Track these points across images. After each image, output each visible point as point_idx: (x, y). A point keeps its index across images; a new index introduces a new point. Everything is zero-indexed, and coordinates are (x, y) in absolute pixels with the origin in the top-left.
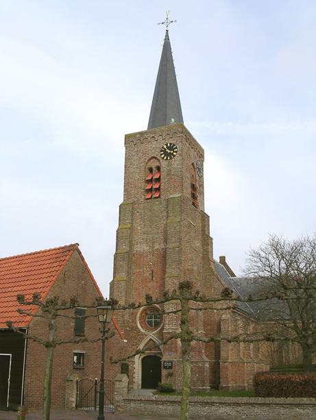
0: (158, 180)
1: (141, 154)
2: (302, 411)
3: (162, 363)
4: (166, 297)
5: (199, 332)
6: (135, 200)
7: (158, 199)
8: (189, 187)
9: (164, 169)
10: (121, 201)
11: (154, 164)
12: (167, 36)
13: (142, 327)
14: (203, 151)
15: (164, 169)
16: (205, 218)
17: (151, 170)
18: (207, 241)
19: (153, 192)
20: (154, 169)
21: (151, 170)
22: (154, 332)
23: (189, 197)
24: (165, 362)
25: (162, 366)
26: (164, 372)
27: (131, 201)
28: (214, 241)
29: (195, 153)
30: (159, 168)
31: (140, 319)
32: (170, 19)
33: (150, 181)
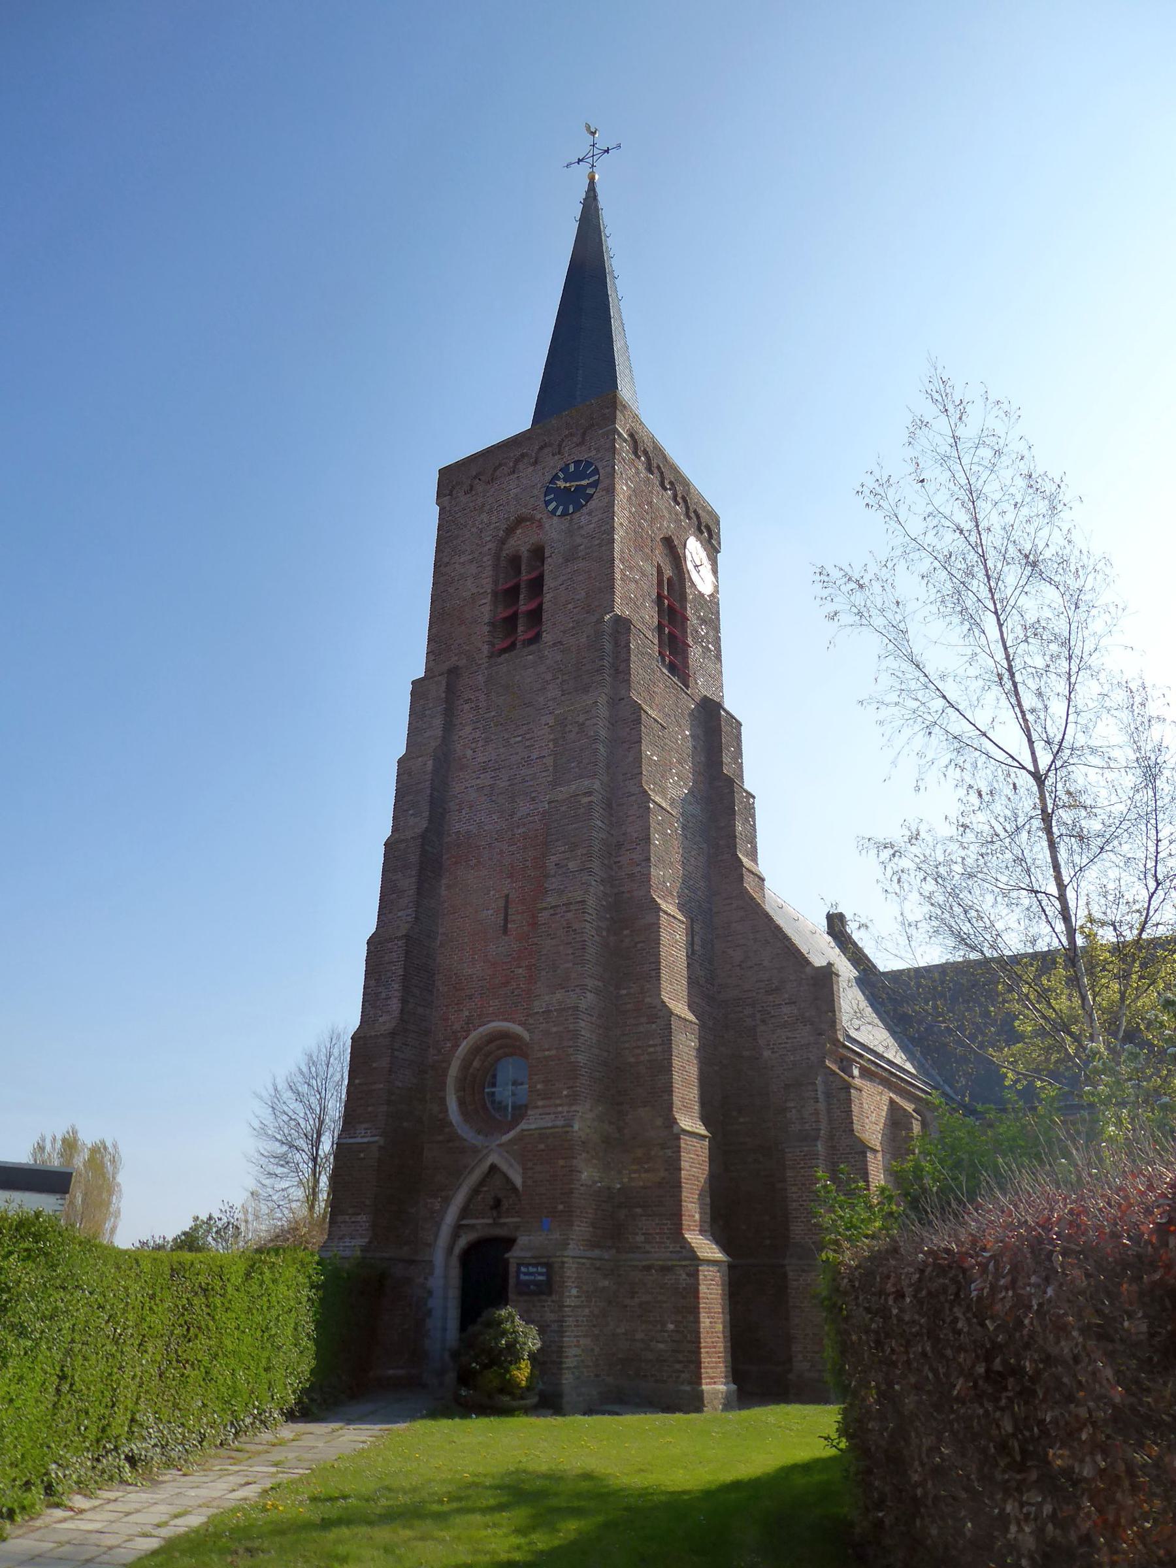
3: (512, 1269)
11: (521, 542)
22: (505, 1138)
25: (512, 1281)
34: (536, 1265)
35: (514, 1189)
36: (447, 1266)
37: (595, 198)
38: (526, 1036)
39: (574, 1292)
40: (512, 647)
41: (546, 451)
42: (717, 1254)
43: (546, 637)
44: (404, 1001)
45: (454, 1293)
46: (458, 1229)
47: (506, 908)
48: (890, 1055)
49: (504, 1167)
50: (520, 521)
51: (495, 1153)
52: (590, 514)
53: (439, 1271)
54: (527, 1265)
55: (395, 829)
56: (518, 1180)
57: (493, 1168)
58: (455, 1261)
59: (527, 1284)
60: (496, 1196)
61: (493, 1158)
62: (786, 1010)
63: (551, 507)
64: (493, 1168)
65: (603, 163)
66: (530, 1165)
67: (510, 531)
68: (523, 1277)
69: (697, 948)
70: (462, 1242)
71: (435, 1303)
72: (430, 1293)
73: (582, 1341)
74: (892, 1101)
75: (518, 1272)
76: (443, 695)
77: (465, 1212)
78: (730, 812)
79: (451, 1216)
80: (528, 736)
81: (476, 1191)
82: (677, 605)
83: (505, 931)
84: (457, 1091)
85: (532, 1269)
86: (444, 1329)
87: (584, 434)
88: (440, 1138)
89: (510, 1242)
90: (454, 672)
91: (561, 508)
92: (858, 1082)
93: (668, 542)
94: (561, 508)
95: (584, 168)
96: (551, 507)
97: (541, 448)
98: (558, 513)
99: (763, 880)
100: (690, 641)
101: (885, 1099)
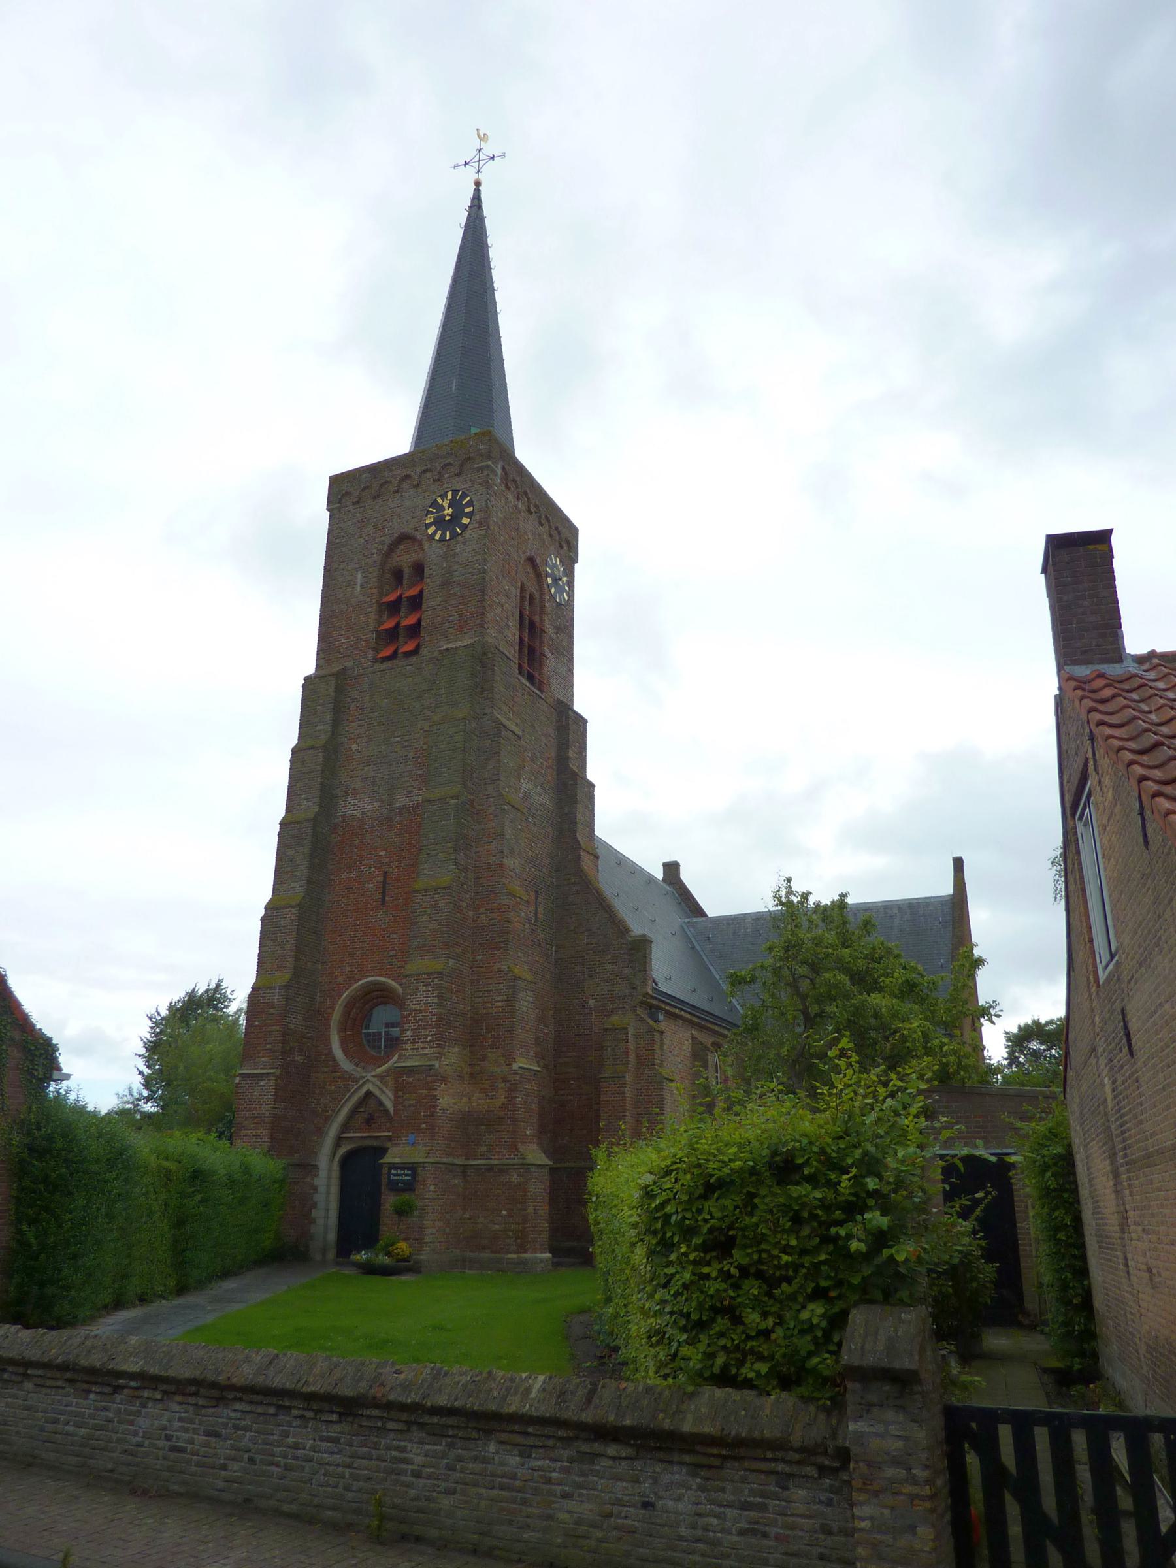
0: (416, 602)
1: (370, 529)
2: (514, 1460)
3: (385, 1170)
4: (689, 1232)
5: (515, 1066)
6: (349, 664)
7: (414, 659)
8: (513, 623)
9: (442, 592)
10: (311, 669)
11: (404, 558)
12: (476, 204)
13: (346, 1051)
14: (574, 531)
15: (442, 592)
16: (569, 731)
17: (398, 575)
18: (572, 792)
19: (401, 639)
20: (407, 572)
21: (398, 575)
22: (379, 1070)
23: (512, 652)
24: (393, 1166)
25: (384, 1181)
26: (389, 1201)
27: (335, 668)
28: (597, 793)
29: (543, 530)
30: (419, 569)
31: (343, 1028)
32: (488, 150)
33: (394, 607)
34: (402, 1169)
35: (386, 1111)
36: (330, 1170)
37: (480, 207)
38: (399, 989)
39: (432, 1188)
40: (394, 656)
41: (428, 475)
42: (543, 1159)
43: (424, 651)
44: (297, 959)
45: (335, 1191)
46: (339, 1141)
47: (384, 882)
48: (1106, 666)
49: (377, 1092)
50: (404, 538)
51: (371, 1080)
52: (464, 543)
53: (323, 1173)
54: (396, 1168)
55: (289, 809)
56: (389, 1105)
57: (369, 1094)
58: (336, 1167)
59: (397, 1182)
60: (368, 1111)
61: (369, 1087)
62: (608, 967)
63: (430, 531)
64: (369, 1094)
65: (489, 170)
66: (400, 1093)
67: (393, 547)
68: (392, 1177)
69: (539, 916)
70: (342, 1151)
71: (319, 1198)
72: (315, 1189)
73: (437, 1223)
74: (693, 1038)
75: (389, 1174)
76: (333, 694)
77: (345, 1127)
78: (573, 801)
79: (333, 1131)
80: (407, 738)
81: (354, 1112)
82: (537, 618)
83: (383, 902)
84: (339, 1032)
85: (399, 1172)
86: (327, 1217)
87: (462, 465)
88: (326, 1070)
89: (383, 1151)
90: (341, 675)
91: (439, 533)
92: (663, 1026)
93: (531, 561)
94: (439, 533)
95: (470, 175)
96: (430, 531)
97: (424, 472)
98: (437, 537)
99: (597, 857)
100: (547, 651)
101: (688, 1035)
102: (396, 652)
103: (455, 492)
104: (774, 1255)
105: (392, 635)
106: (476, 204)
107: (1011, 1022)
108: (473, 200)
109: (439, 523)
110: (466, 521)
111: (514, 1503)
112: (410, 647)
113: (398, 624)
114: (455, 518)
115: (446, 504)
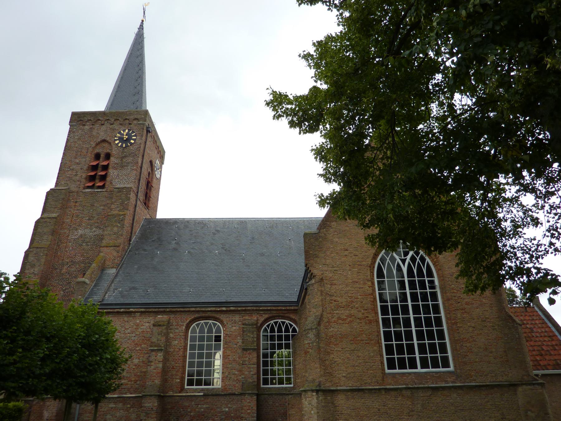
12: (141, 27)
15: (111, 152)
17: (97, 156)
20: (102, 156)
63: (117, 142)
96: (117, 142)
102: (94, 185)
103: (129, 130)
104: (334, 209)
105: (92, 178)
106: (141, 27)
107: (454, 253)
108: (140, 25)
109: (121, 139)
110: (132, 141)
111: (381, 301)
112: (100, 184)
113: (96, 174)
114: (128, 140)
115: (125, 134)
